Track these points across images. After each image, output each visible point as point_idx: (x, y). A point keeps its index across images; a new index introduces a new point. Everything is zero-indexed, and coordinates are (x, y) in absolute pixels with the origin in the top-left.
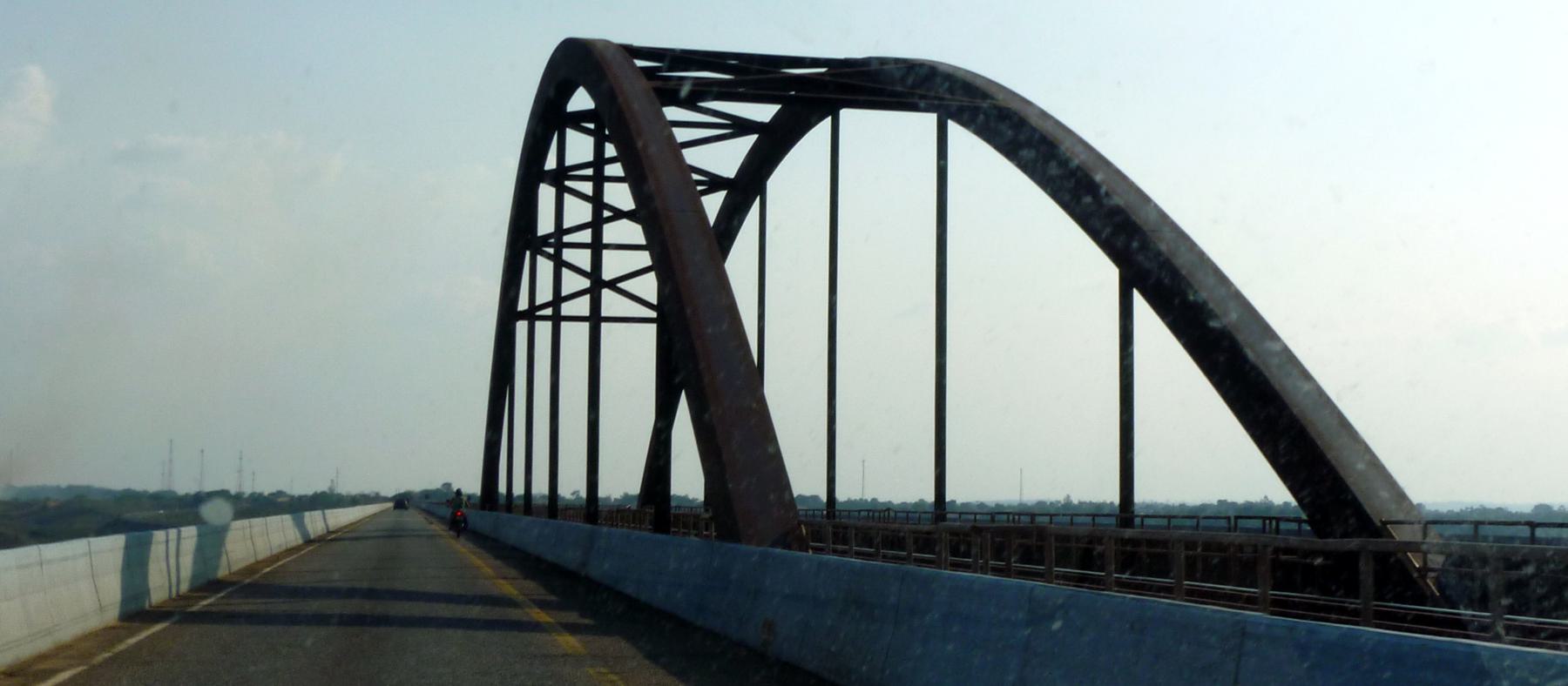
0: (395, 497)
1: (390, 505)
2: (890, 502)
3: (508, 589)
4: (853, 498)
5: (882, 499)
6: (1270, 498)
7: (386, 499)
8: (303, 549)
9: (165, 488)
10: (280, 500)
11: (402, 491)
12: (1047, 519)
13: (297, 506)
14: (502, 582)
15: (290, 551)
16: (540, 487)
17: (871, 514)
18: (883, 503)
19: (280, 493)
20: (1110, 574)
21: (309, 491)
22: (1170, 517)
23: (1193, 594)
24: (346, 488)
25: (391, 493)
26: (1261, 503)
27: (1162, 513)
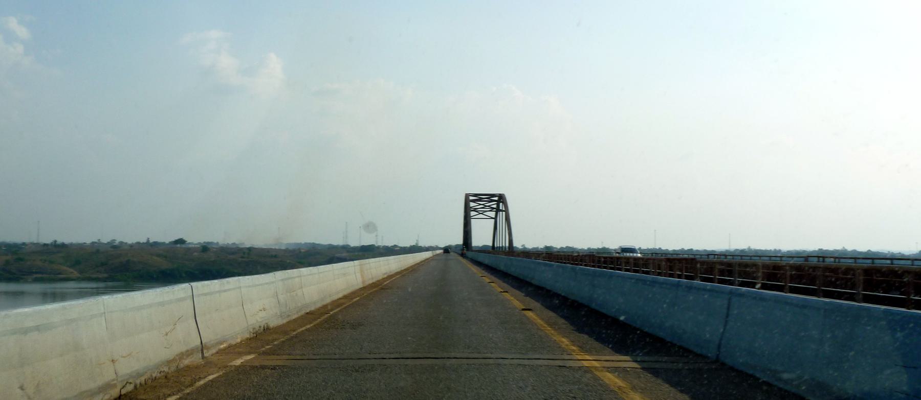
0: (444, 248)
1: (441, 251)
2: (667, 250)
3: (546, 326)
4: (650, 248)
5: (664, 248)
6: (846, 248)
7: (440, 249)
8: (395, 277)
9: (345, 244)
10: (396, 249)
11: (447, 245)
12: (816, 259)
13: (427, 249)
14: (608, 373)
15: (431, 257)
16: (504, 245)
17: (837, 260)
18: (664, 250)
19: (395, 246)
20: (715, 276)
21: (408, 245)
22: (891, 259)
23: (867, 299)
24: (422, 244)
25: (443, 246)
26: (842, 251)
27: (888, 256)
